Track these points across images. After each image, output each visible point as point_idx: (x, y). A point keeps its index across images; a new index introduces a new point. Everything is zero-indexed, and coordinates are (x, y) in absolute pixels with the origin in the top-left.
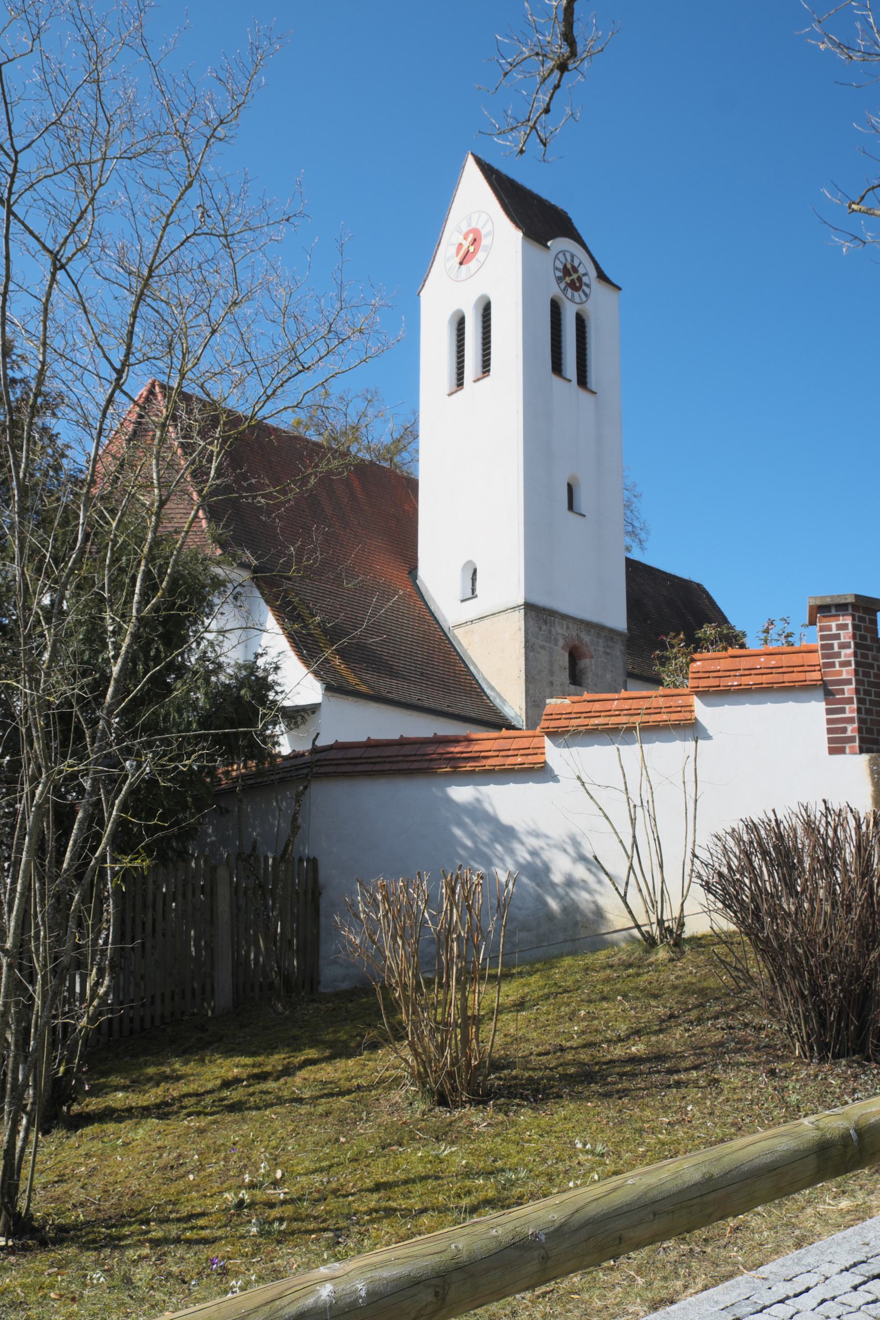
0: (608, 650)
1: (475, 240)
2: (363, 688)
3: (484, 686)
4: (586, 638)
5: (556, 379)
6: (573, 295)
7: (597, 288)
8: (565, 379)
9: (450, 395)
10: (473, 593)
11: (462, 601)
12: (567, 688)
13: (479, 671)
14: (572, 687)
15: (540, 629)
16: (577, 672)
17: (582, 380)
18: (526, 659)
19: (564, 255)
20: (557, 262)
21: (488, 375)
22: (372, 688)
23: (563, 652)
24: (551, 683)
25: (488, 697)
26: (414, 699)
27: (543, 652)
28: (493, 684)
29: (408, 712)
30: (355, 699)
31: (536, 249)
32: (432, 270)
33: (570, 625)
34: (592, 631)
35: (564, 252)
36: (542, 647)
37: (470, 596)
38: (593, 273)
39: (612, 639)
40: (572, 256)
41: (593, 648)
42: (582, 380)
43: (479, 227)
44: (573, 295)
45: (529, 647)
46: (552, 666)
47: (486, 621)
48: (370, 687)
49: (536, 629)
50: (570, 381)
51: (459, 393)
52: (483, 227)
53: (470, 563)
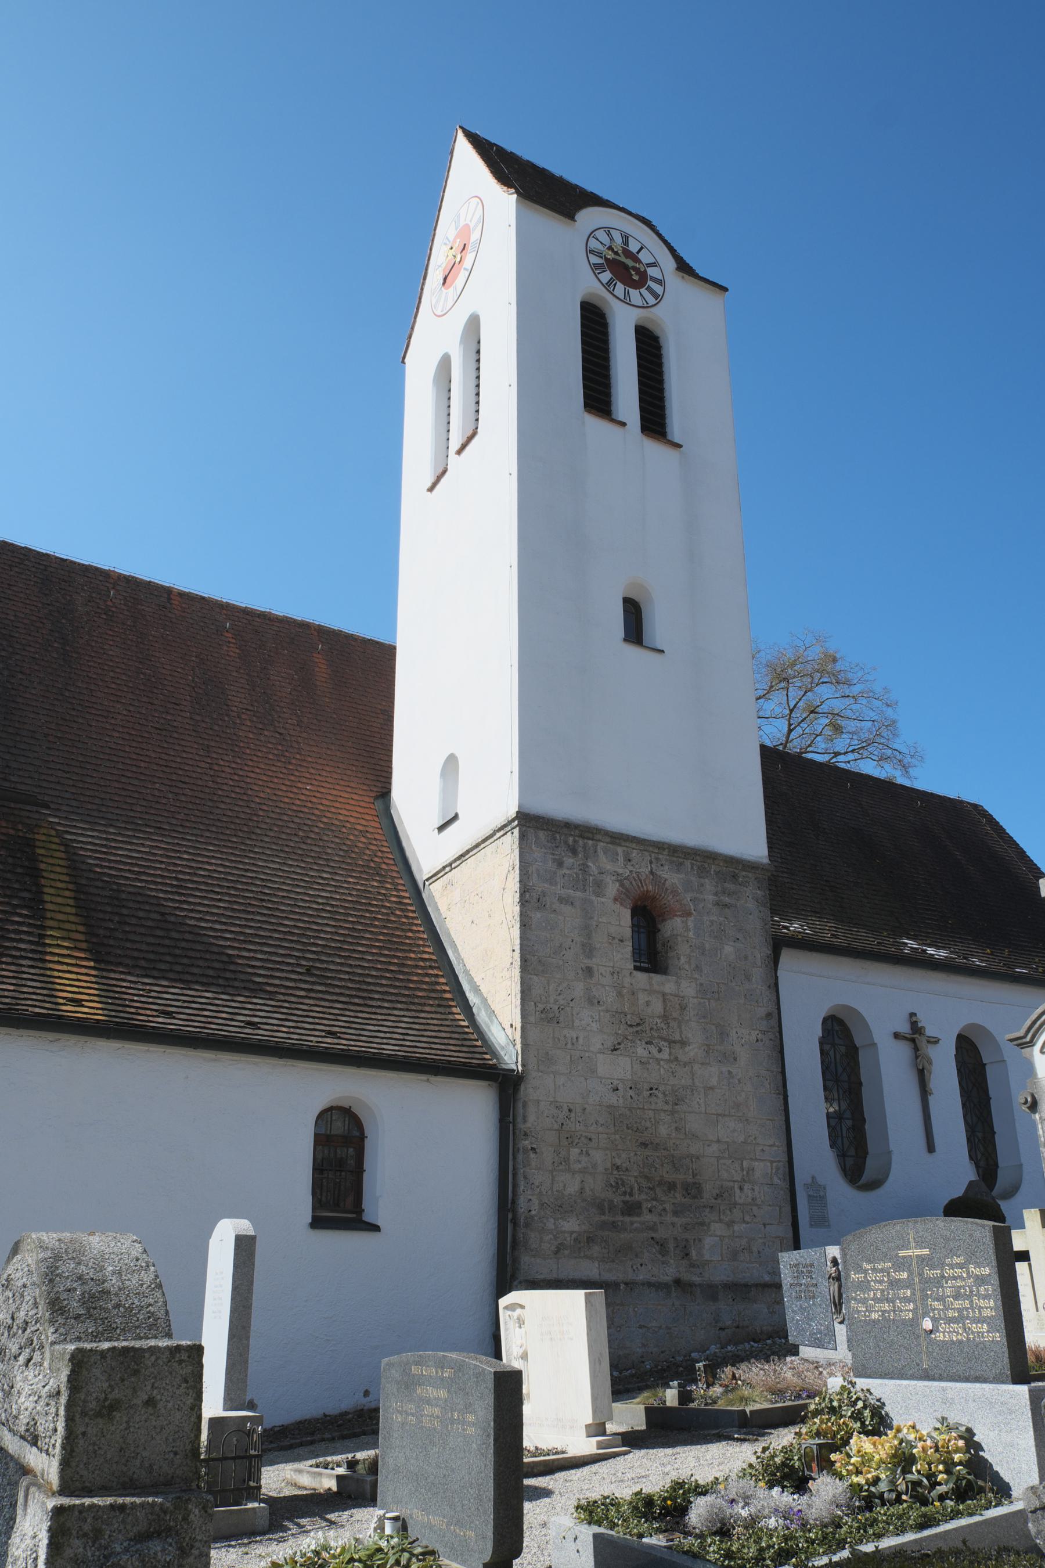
0: (726, 900)
3: (466, 987)
4: (672, 877)
5: (594, 424)
6: (627, 294)
7: (675, 283)
11: (441, 828)
12: (627, 980)
14: (642, 978)
15: (560, 864)
16: (659, 947)
18: (525, 924)
19: (609, 234)
20: (592, 241)
23: (617, 906)
24: (589, 971)
27: (567, 909)
28: (477, 980)
31: (547, 223)
34: (688, 863)
38: (668, 264)
39: (734, 877)
41: (689, 896)
44: (627, 294)
46: (589, 936)
49: (550, 865)
50: (623, 424)
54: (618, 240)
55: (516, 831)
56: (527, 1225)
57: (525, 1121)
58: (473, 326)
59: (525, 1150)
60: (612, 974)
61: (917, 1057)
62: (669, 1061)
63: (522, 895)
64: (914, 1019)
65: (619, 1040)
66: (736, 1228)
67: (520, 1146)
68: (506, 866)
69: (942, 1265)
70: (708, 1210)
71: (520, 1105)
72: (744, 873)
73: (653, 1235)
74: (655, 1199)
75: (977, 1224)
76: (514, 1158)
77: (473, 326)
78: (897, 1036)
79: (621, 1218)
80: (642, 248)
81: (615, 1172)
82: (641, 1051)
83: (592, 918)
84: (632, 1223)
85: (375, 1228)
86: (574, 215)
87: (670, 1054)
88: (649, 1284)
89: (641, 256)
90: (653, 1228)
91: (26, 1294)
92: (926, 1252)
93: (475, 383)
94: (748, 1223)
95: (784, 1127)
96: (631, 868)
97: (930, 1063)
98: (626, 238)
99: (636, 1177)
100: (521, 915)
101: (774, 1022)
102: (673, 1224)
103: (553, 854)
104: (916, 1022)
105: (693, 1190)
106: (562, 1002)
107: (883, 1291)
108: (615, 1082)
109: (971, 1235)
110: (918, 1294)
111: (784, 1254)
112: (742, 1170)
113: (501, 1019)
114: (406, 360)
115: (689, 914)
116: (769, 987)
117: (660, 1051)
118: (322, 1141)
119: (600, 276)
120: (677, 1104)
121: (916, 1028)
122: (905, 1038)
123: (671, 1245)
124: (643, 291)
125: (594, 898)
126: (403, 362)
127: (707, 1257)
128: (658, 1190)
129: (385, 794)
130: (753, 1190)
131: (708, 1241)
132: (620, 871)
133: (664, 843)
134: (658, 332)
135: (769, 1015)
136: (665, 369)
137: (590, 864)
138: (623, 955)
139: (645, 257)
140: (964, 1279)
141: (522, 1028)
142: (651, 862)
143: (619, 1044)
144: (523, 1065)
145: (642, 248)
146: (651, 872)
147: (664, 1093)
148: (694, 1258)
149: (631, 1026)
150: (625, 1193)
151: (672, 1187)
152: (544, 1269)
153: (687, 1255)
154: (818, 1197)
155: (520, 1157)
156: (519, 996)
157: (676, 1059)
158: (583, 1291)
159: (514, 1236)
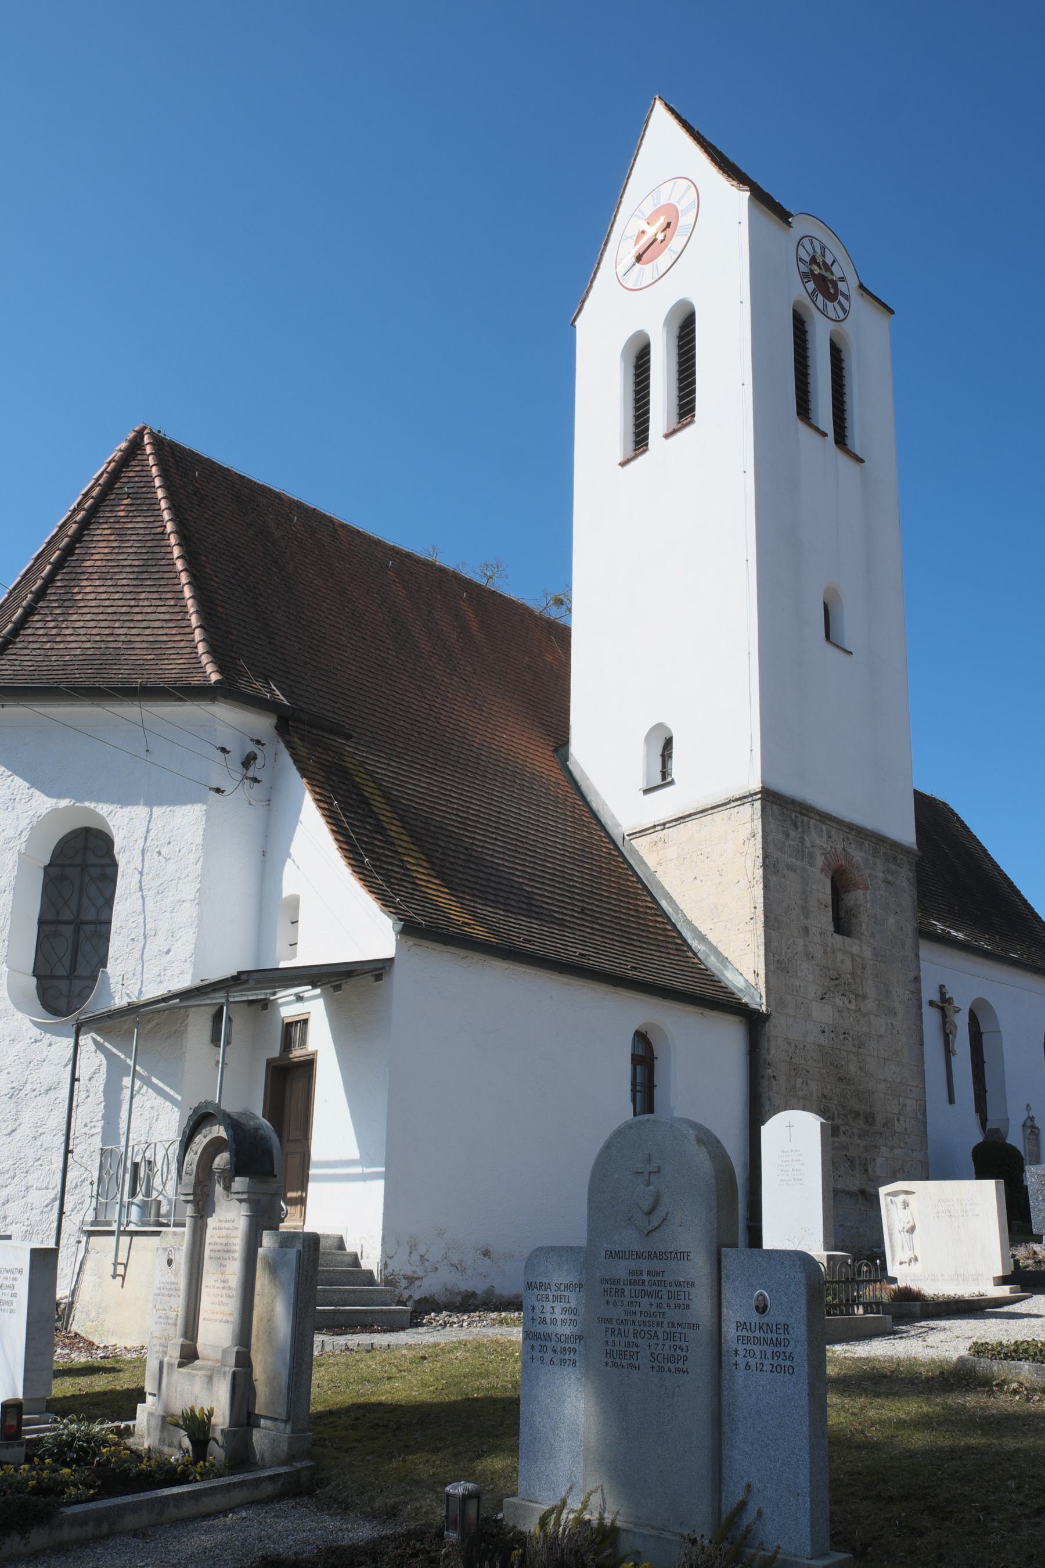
1: (668, 225)
2: (479, 932)
4: (858, 856)
6: (825, 305)
7: (858, 304)
8: (817, 430)
9: (623, 464)
10: (664, 778)
11: (646, 791)
13: (676, 908)
15: (787, 836)
17: (841, 438)
19: (812, 243)
21: (692, 422)
22: (496, 932)
24: (806, 930)
25: (695, 954)
26: (574, 953)
28: (703, 929)
29: (563, 979)
30: (463, 953)
32: (595, 284)
33: (833, 832)
34: (866, 843)
35: (811, 238)
36: (791, 867)
37: (659, 782)
40: (823, 248)
41: (867, 872)
42: (841, 438)
43: (673, 201)
44: (825, 305)
45: (770, 865)
47: (692, 825)
48: (491, 930)
49: (781, 836)
50: (824, 435)
51: (641, 459)
52: (678, 202)
53: (660, 727)
114: (577, 323)
126: (573, 324)
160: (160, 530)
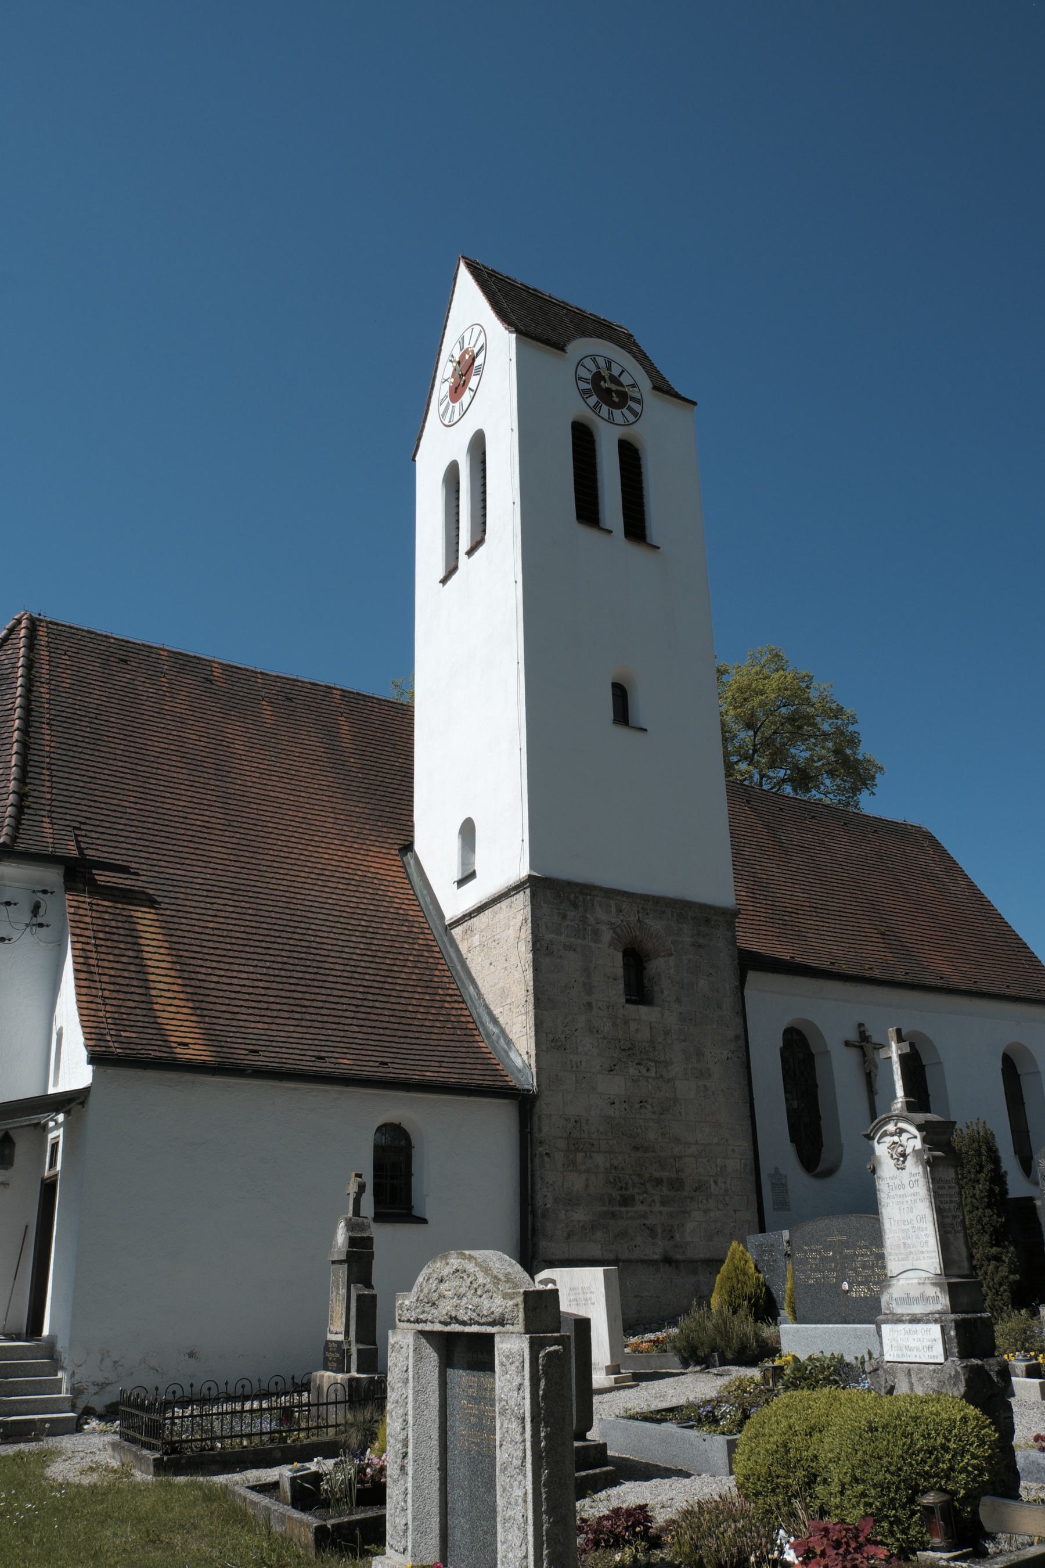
4: (655, 925)
5: (586, 533)
7: (653, 405)
8: (602, 529)
15: (564, 917)
16: (646, 981)
19: (594, 361)
20: (581, 369)
24: (589, 1005)
28: (496, 1012)
31: (544, 357)
38: (645, 384)
39: (707, 921)
40: (609, 363)
50: (610, 532)
54: (602, 363)
55: (528, 891)
56: (544, 1216)
57: (540, 1131)
58: (478, 446)
59: (541, 1156)
60: (608, 1007)
61: (865, 1062)
62: (656, 1078)
63: (533, 945)
64: (862, 1029)
65: (615, 1062)
66: (712, 1214)
67: (537, 1152)
68: (520, 918)
69: (854, 1247)
70: (688, 1200)
71: (536, 1119)
72: (715, 918)
73: (646, 1222)
74: (646, 1192)
75: (870, 1218)
76: (532, 1161)
77: (478, 446)
78: (847, 1044)
79: (618, 1208)
80: (623, 372)
81: (613, 1171)
82: (632, 1071)
83: (591, 961)
84: (628, 1212)
85: (424, 1221)
86: (565, 346)
87: (656, 1072)
88: (643, 1262)
89: (622, 379)
90: (644, 1216)
91: (1000, 1269)
92: (845, 1238)
93: (481, 483)
94: (721, 1210)
95: (750, 1130)
96: (622, 918)
97: (876, 1067)
98: (609, 363)
99: (630, 1175)
100: (534, 961)
101: (741, 1042)
102: (661, 1212)
103: (558, 909)
104: (864, 1031)
105: (677, 1184)
106: (568, 1032)
107: (816, 1265)
108: (612, 1097)
109: (873, 1226)
110: (839, 1266)
111: (751, 1237)
112: (717, 1166)
113: (518, 1046)
114: (417, 458)
115: (671, 955)
116: (737, 1013)
117: (648, 1070)
118: (379, 1150)
119: (588, 400)
120: (662, 1114)
121: (864, 1037)
122: (855, 1046)
123: (659, 1230)
124: (625, 410)
125: (592, 944)
126: (414, 460)
127: (689, 1239)
128: (648, 1185)
129: (408, 847)
130: (725, 1183)
131: (690, 1226)
132: (613, 920)
133: (648, 896)
134: (638, 446)
135: (737, 1037)
136: (643, 470)
137: (589, 916)
138: (617, 992)
139: (625, 380)
140: (868, 1256)
141: (537, 1055)
142: (638, 912)
143: (615, 1065)
144: (538, 1086)
145: (623, 372)
146: (639, 920)
147: (652, 1105)
148: (678, 1240)
149: (624, 1050)
150: (621, 1188)
151: (659, 1182)
152: (557, 1249)
153: (672, 1237)
154: (780, 1185)
155: (537, 1160)
156: (533, 1029)
157: (661, 1077)
158: (602, 1269)
159: (533, 1225)
160: (10, 706)
